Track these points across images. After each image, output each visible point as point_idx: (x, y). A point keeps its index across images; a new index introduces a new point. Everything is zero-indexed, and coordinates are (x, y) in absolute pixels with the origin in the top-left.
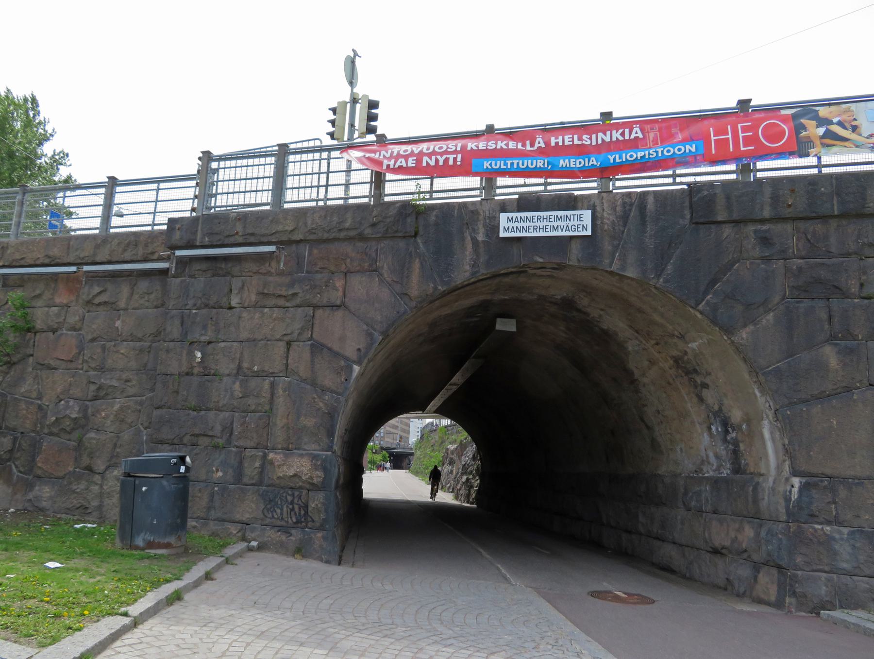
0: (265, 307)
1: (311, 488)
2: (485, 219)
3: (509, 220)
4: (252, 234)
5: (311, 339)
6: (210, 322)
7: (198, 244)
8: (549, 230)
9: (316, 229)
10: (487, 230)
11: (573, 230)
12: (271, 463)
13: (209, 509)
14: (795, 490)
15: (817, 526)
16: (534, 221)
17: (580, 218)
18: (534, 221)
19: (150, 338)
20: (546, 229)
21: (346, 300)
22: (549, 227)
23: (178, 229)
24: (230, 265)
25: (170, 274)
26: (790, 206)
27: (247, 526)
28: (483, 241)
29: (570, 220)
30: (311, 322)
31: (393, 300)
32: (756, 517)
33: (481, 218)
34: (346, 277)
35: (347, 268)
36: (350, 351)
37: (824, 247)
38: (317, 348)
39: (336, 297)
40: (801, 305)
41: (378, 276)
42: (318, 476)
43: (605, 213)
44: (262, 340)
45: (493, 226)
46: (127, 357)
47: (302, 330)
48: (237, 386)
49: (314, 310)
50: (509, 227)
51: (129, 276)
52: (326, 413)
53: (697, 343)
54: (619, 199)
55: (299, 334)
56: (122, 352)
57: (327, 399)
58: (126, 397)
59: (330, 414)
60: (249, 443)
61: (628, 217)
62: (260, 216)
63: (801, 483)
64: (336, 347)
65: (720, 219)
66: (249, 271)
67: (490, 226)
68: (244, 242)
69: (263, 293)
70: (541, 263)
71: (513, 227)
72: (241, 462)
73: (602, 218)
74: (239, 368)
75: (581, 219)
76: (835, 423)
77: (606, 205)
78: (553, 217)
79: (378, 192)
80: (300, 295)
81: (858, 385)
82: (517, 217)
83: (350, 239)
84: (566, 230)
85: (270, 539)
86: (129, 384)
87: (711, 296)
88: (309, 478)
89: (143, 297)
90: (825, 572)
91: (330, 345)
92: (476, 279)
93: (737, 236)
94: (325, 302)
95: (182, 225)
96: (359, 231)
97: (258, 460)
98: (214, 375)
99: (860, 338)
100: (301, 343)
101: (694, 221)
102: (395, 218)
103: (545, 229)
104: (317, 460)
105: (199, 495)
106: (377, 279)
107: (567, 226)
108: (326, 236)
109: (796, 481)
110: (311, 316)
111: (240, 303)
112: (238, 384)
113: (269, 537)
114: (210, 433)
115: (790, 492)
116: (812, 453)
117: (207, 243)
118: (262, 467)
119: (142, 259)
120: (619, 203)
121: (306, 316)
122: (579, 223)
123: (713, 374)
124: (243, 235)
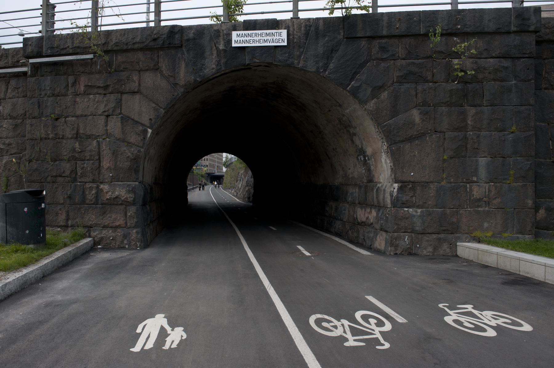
0: (90, 94)
1: (128, 204)
2: (224, 35)
3: (238, 36)
4: (79, 47)
5: (121, 113)
6: (56, 105)
7: (44, 55)
8: (262, 42)
9: (118, 43)
10: (225, 43)
11: (276, 42)
12: (102, 190)
13: (67, 220)
14: (396, 190)
15: (405, 209)
16: (253, 36)
17: (280, 34)
18: (253, 36)
19: (21, 117)
20: (262, 35)
21: (141, 88)
22: (262, 40)
23: (30, 45)
24: (66, 68)
25: (28, 75)
26: (397, 28)
27: (91, 229)
28: (223, 49)
29: (274, 36)
30: (119, 103)
31: (170, 88)
32: (379, 207)
33: (221, 34)
34: (140, 74)
35: (140, 68)
36: (145, 120)
37: (415, 53)
38: (125, 119)
39: (134, 86)
40: (402, 87)
41: (160, 72)
42: (130, 197)
43: (295, 31)
44: (90, 115)
45: (229, 39)
46: (8, 129)
47: (115, 108)
48: (77, 145)
49: (121, 95)
50: (238, 40)
51: (4, 77)
52: (133, 159)
53: (349, 110)
54: (303, 23)
55: (113, 111)
56: (4, 126)
57: (133, 150)
58: (10, 155)
59: (135, 159)
60: (87, 179)
61: (308, 34)
62: (84, 36)
63: (398, 187)
64: (136, 119)
65: (359, 35)
66: (79, 72)
67: (227, 40)
68: (74, 52)
69: (88, 85)
70: (258, 63)
71: (240, 40)
72: (84, 192)
73: (293, 35)
74: (77, 133)
75: (281, 35)
76: (417, 153)
77: (295, 26)
78: (264, 34)
79: (157, 18)
80: (111, 86)
81: (429, 132)
82: (242, 34)
83: (141, 49)
84: (272, 42)
85: (105, 235)
86: (11, 147)
87: (354, 82)
88: (125, 199)
89: (14, 91)
90: (409, 233)
91: (132, 117)
92: (220, 74)
93: (369, 46)
94: (127, 90)
95: (32, 42)
96: (146, 44)
97: (94, 189)
98: (62, 138)
99: (432, 105)
100: (115, 117)
101: (345, 37)
102: (167, 35)
103: (259, 41)
104: (129, 188)
105: (60, 212)
106: (159, 75)
107: (273, 39)
108: (125, 47)
109: (396, 185)
110: (119, 99)
111: (75, 93)
112: (77, 143)
113: (105, 234)
114: (64, 175)
115: (393, 192)
116: (404, 170)
117: (50, 54)
118: (97, 193)
119: (12, 65)
120: (303, 26)
121: (117, 99)
122: (280, 37)
123: (357, 127)
124: (72, 48)
